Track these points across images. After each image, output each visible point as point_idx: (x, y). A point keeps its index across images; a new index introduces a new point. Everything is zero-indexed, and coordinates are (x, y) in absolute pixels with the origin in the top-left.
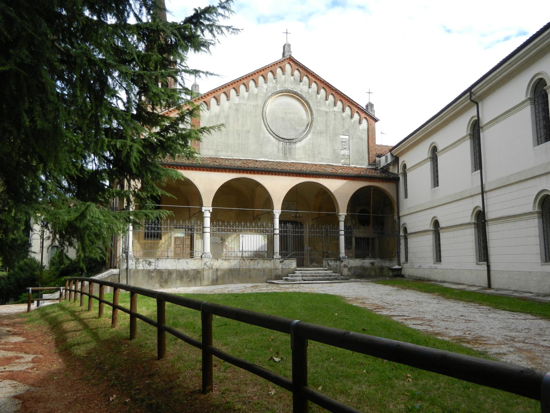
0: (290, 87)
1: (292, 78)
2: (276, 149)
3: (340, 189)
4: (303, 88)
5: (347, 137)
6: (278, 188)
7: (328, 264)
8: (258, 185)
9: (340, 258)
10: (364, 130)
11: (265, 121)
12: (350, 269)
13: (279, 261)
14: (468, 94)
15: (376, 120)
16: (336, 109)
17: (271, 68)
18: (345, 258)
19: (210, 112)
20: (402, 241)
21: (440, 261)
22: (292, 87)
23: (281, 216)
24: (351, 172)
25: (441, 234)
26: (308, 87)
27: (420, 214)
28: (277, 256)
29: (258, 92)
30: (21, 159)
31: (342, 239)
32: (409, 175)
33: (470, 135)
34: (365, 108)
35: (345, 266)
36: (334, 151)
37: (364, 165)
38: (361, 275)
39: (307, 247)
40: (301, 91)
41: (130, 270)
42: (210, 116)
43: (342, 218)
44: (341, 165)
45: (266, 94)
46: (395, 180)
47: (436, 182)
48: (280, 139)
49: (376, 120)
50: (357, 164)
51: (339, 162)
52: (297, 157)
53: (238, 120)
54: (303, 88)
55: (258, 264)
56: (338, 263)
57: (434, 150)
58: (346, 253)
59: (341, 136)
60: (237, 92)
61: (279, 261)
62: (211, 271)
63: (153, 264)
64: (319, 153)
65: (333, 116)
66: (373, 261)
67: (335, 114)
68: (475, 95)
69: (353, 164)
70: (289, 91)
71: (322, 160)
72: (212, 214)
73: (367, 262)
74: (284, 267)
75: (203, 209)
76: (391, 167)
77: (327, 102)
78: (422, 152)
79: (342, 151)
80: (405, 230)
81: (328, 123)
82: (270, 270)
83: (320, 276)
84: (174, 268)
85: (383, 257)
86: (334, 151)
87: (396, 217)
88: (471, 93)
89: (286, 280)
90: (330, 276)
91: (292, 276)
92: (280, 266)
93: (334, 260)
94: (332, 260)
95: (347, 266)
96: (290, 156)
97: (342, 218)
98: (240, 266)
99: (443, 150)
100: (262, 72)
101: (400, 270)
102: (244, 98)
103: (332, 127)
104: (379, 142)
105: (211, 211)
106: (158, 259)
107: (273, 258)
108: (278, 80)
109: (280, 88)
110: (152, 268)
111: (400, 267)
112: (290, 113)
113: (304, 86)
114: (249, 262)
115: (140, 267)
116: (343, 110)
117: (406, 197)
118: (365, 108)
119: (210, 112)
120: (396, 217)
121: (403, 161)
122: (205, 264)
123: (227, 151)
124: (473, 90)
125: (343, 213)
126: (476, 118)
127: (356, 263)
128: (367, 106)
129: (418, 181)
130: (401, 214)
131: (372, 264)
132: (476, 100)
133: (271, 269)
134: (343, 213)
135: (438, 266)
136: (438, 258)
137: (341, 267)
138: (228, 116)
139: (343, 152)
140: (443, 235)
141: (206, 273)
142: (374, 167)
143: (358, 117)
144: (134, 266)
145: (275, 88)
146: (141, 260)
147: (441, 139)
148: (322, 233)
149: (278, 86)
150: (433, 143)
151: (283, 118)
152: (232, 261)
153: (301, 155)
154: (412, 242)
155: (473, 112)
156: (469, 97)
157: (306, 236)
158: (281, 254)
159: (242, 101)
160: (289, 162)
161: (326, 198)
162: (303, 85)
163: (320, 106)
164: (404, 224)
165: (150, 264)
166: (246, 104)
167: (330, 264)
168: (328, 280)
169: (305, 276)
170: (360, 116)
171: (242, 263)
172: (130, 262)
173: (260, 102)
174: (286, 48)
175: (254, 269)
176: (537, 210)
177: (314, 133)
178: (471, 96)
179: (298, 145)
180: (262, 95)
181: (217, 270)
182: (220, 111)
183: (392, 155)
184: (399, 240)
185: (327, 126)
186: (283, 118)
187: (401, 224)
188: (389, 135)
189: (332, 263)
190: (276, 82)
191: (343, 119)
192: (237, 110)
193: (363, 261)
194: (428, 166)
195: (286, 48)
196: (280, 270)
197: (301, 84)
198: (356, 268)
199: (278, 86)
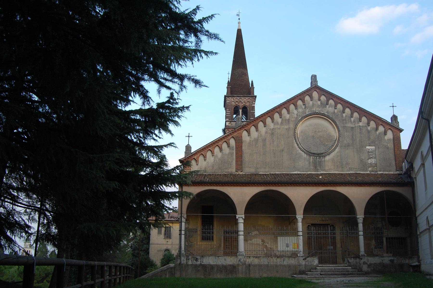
0: (317, 110)
1: (319, 103)
2: (307, 163)
3: (359, 196)
5: (374, 147)
6: (299, 196)
7: (348, 261)
10: (389, 140)
13: (302, 258)
15: (401, 131)
17: (301, 96)
18: (364, 256)
19: (251, 138)
22: (320, 110)
24: (360, 179)
26: (333, 108)
29: (290, 117)
30: (16, 194)
34: (390, 121)
35: (364, 263)
36: (361, 160)
37: (393, 172)
40: (328, 112)
41: (182, 265)
42: (250, 141)
44: (368, 172)
45: (296, 118)
49: (401, 131)
50: (384, 171)
51: (367, 171)
53: (273, 142)
55: (284, 261)
56: (358, 260)
59: (367, 147)
60: (273, 119)
61: (302, 258)
62: (244, 266)
63: (199, 260)
64: (347, 164)
65: (359, 131)
66: (392, 258)
67: (360, 129)
70: (317, 114)
71: (350, 169)
74: (307, 264)
77: (352, 119)
79: (369, 160)
81: (354, 137)
83: (338, 272)
84: (215, 263)
86: (361, 160)
92: (303, 263)
93: (353, 257)
94: (351, 257)
95: (367, 263)
96: (320, 167)
102: (278, 124)
103: (358, 140)
105: (244, 218)
106: (203, 256)
108: (307, 106)
109: (309, 112)
110: (199, 263)
112: (319, 132)
113: (330, 108)
114: (276, 260)
115: (190, 262)
119: (251, 138)
122: (239, 260)
123: (265, 168)
125: (360, 217)
131: (392, 261)
134: (360, 217)
137: (360, 264)
138: (265, 140)
141: (240, 268)
143: (383, 129)
144: (185, 261)
145: (304, 112)
146: (190, 257)
149: (307, 110)
152: (261, 258)
153: (330, 166)
154: (360, 236)
159: (276, 126)
161: (347, 204)
162: (329, 107)
163: (346, 123)
165: (197, 260)
166: (279, 129)
167: (350, 261)
170: (384, 127)
171: (270, 260)
172: (182, 258)
173: (292, 126)
174: (314, 78)
175: (281, 265)
177: (341, 147)
179: (327, 158)
180: (293, 119)
181: (249, 265)
182: (258, 136)
189: (352, 260)
190: (305, 108)
191: (369, 132)
192: (273, 134)
195: (314, 78)
196: (304, 266)
197: (328, 106)
198: (375, 264)
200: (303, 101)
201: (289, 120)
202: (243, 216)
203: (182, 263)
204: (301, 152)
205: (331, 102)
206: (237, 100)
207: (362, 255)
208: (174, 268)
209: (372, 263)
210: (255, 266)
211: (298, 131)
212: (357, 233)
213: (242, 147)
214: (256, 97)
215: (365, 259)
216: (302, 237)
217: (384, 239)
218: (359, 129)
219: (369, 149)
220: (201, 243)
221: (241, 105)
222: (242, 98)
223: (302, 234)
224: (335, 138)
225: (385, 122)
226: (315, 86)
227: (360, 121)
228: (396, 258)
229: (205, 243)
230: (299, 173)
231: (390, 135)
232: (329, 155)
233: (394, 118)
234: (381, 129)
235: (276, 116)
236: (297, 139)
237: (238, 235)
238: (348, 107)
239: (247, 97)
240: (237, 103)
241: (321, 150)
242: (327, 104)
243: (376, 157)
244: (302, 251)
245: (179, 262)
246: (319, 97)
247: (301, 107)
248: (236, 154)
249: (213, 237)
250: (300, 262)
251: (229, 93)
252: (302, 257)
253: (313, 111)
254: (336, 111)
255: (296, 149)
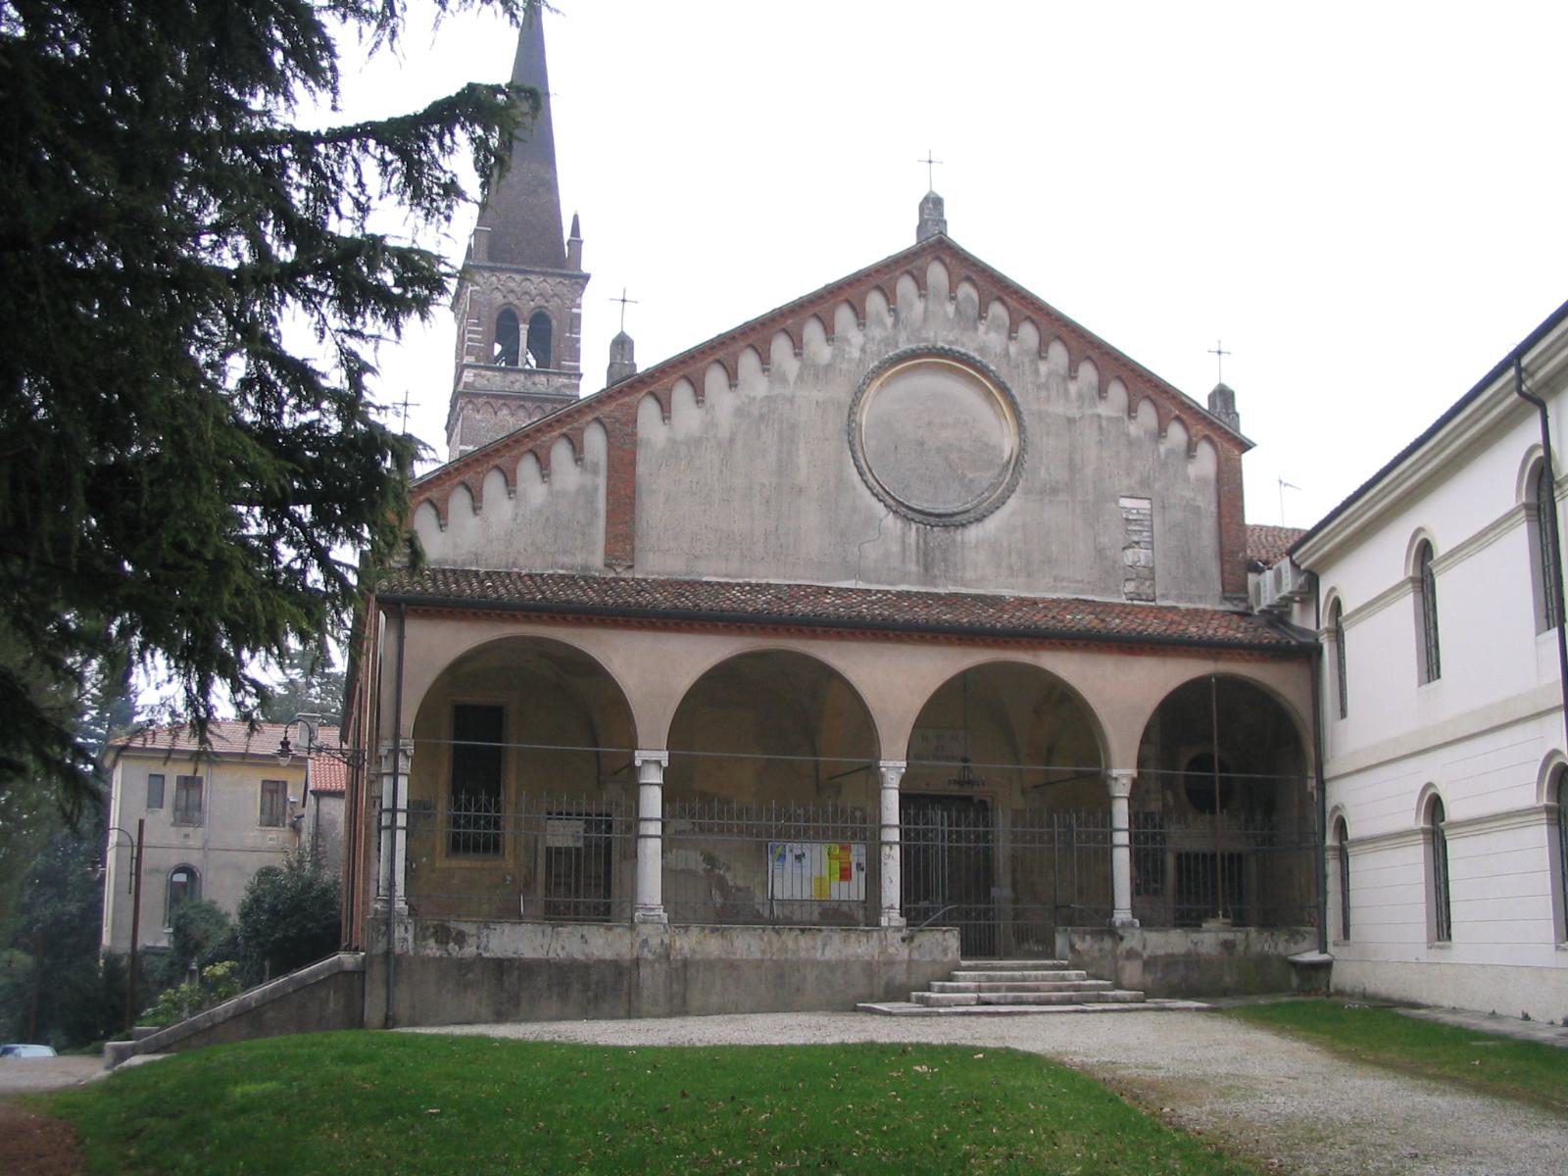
1: (950, 309)
2: (895, 548)
3: (1124, 694)
4: (988, 340)
5: (1145, 504)
6: (896, 684)
7: (1072, 947)
8: (832, 674)
9: (1112, 925)
10: (1202, 480)
11: (860, 454)
12: (1149, 964)
13: (898, 936)
14: (1512, 372)
15: (1245, 446)
16: (1102, 409)
17: (880, 278)
18: (1132, 925)
20: (1332, 867)
21: (1449, 937)
22: (951, 337)
23: (904, 780)
25: (1449, 844)
26: (1004, 337)
27: (1357, 777)
28: (892, 918)
29: (834, 357)
31: (1122, 860)
32: (1349, 636)
33: (1527, 506)
34: (1206, 406)
35: (1131, 954)
36: (1100, 551)
38: (1179, 984)
39: (1002, 891)
43: (1121, 790)
44: (1123, 600)
46: (1306, 654)
47: (1431, 669)
48: (911, 515)
49: (1245, 446)
50: (1179, 597)
51: (1118, 593)
52: (970, 574)
54: (988, 340)
55: (824, 946)
56: (1108, 943)
57: (1424, 551)
58: (1133, 908)
59: (1125, 502)
61: (898, 936)
63: (472, 941)
66: (1229, 936)
67: (1100, 428)
68: (1532, 375)
69: (1164, 596)
72: (667, 773)
73: (1210, 938)
74: (916, 956)
75: (639, 757)
76: (1296, 607)
78: (1384, 562)
79: (1129, 552)
80: (1341, 826)
82: (869, 968)
84: (540, 954)
85: (1270, 922)
86: (1100, 551)
87: (1312, 783)
88: (1520, 370)
89: (925, 1001)
90: (1077, 988)
91: (942, 990)
92: (902, 952)
93: (1092, 934)
94: (1085, 933)
97: (1121, 790)
98: (763, 952)
99: (1451, 554)
100: (849, 292)
101: (1326, 967)
104: (1252, 517)
105: (665, 764)
107: (878, 924)
108: (903, 315)
109: (909, 340)
111: (1324, 957)
113: (992, 335)
116: (1131, 411)
117: (1343, 713)
118: (1206, 406)
120: (1312, 783)
121: (1333, 589)
124: (1525, 361)
125: (1123, 773)
126: (1540, 453)
127: (1173, 942)
128: (1212, 398)
129: (1375, 657)
130: (1328, 773)
131: (1228, 945)
132: (1540, 395)
133: (869, 964)
134: (1123, 773)
135: (1436, 956)
136: (1442, 927)
139: (1130, 556)
140: (1455, 848)
142: (1241, 608)
147: (1446, 517)
148: (1052, 840)
150: (1420, 530)
151: (921, 443)
153: (989, 565)
154: (1362, 866)
155: (1529, 434)
156: (1514, 384)
157: (1003, 848)
158: (904, 912)
159: (778, 390)
160: (941, 591)
163: (1048, 399)
164: (1336, 808)
167: (1079, 946)
168: (1069, 1001)
169: (991, 990)
171: (770, 942)
172: (399, 932)
173: (841, 391)
174: (932, 206)
176: (1545, 801)
177: (1027, 492)
178: (1520, 381)
179: (973, 533)
183: (1295, 565)
184: (1321, 863)
185: (1072, 467)
186: (921, 443)
187: (1329, 809)
188: (1285, 493)
193: (1195, 936)
194: (1407, 606)
195: (932, 206)
199: (903, 337)
200: (890, 297)
201: (828, 367)
202: (664, 757)
203: (398, 950)
204: (874, 500)
205: (997, 310)
206: (512, 285)
207: (1123, 924)
208: (361, 972)
209: (1160, 952)
210: (710, 965)
211: (864, 418)
212: (1108, 838)
213: (633, 463)
214: (587, 278)
215: (1133, 940)
216: (897, 848)
217: (1170, 861)
218: (1095, 426)
219: (1128, 510)
220: (446, 864)
221: (526, 307)
222: (532, 277)
223: (1126, 841)
224: (1006, 455)
225: (1190, 408)
226: (935, 246)
227: (1101, 397)
228: (1240, 936)
229: (466, 864)
230: (862, 585)
231: (1206, 461)
232: (979, 520)
233: (1224, 396)
234: (1176, 434)
235: (781, 347)
236: (857, 447)
237: (639, 836)
238: (1059, 338)
239: (552, 275)
240: (511, 298)
241: (949, 501)
242: (981, 317)
243: (1152, 543)
244: (897, 906)
245: (380, 947)
246: (953, 288)
247: (881, 323)
248: (609, 494)
249: (497, 838)
250: (891, 950)
251: (483, 255)
252: (899, 929)
253: (927, 340)
254: (1013, 349)
255: (854, 488)
